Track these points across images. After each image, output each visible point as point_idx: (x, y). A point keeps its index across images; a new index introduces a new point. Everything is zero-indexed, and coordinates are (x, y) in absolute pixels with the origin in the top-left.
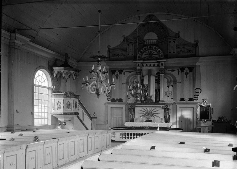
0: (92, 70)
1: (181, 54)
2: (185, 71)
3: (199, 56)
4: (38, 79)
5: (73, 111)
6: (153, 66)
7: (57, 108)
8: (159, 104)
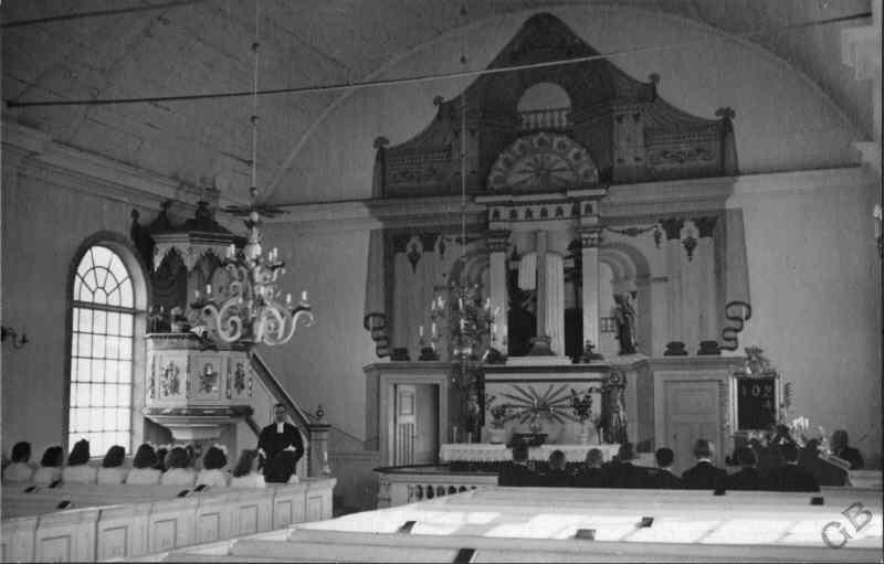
0: (228, 256)
1: (666, 165)
2: (684, 235)
3: (737, 173)
4: (90, 279)
5: (225, 403)
6: (523, 218)
7: (162, 390)
8: (591, 367)
